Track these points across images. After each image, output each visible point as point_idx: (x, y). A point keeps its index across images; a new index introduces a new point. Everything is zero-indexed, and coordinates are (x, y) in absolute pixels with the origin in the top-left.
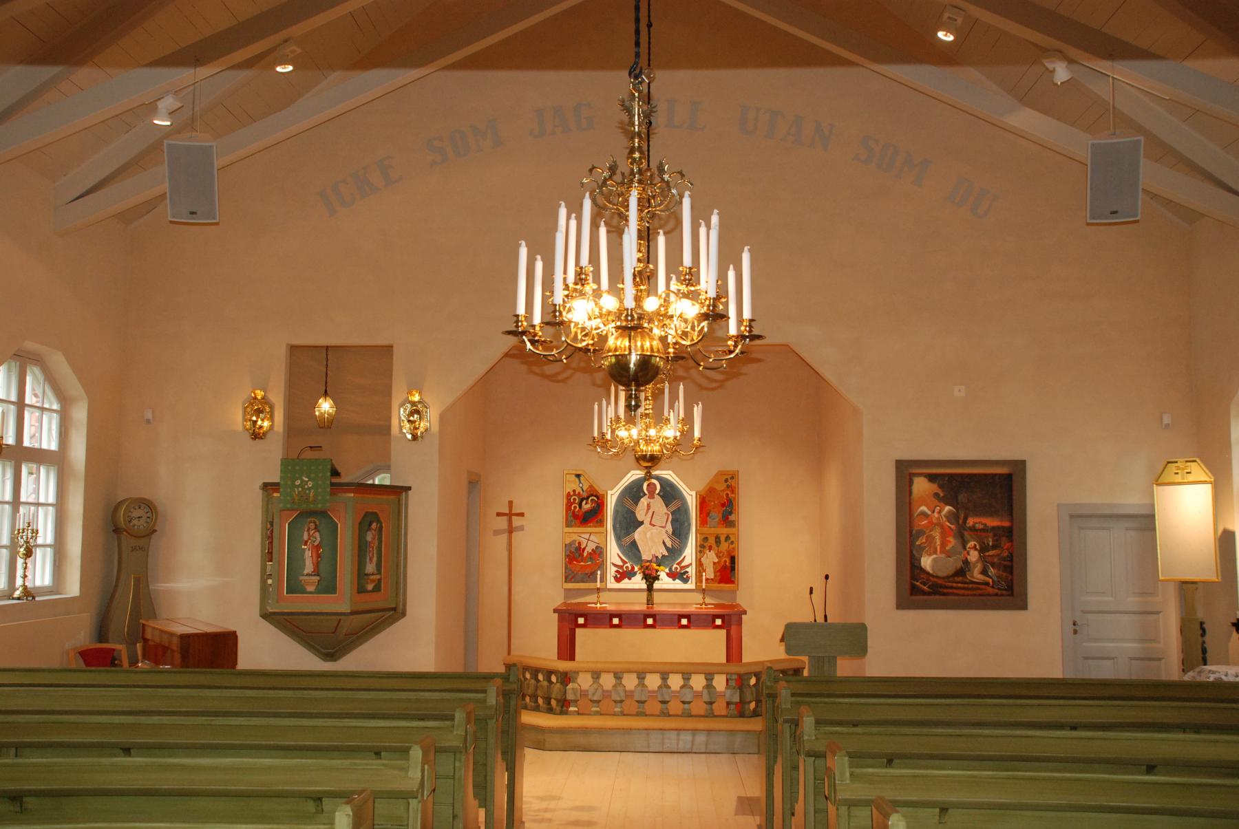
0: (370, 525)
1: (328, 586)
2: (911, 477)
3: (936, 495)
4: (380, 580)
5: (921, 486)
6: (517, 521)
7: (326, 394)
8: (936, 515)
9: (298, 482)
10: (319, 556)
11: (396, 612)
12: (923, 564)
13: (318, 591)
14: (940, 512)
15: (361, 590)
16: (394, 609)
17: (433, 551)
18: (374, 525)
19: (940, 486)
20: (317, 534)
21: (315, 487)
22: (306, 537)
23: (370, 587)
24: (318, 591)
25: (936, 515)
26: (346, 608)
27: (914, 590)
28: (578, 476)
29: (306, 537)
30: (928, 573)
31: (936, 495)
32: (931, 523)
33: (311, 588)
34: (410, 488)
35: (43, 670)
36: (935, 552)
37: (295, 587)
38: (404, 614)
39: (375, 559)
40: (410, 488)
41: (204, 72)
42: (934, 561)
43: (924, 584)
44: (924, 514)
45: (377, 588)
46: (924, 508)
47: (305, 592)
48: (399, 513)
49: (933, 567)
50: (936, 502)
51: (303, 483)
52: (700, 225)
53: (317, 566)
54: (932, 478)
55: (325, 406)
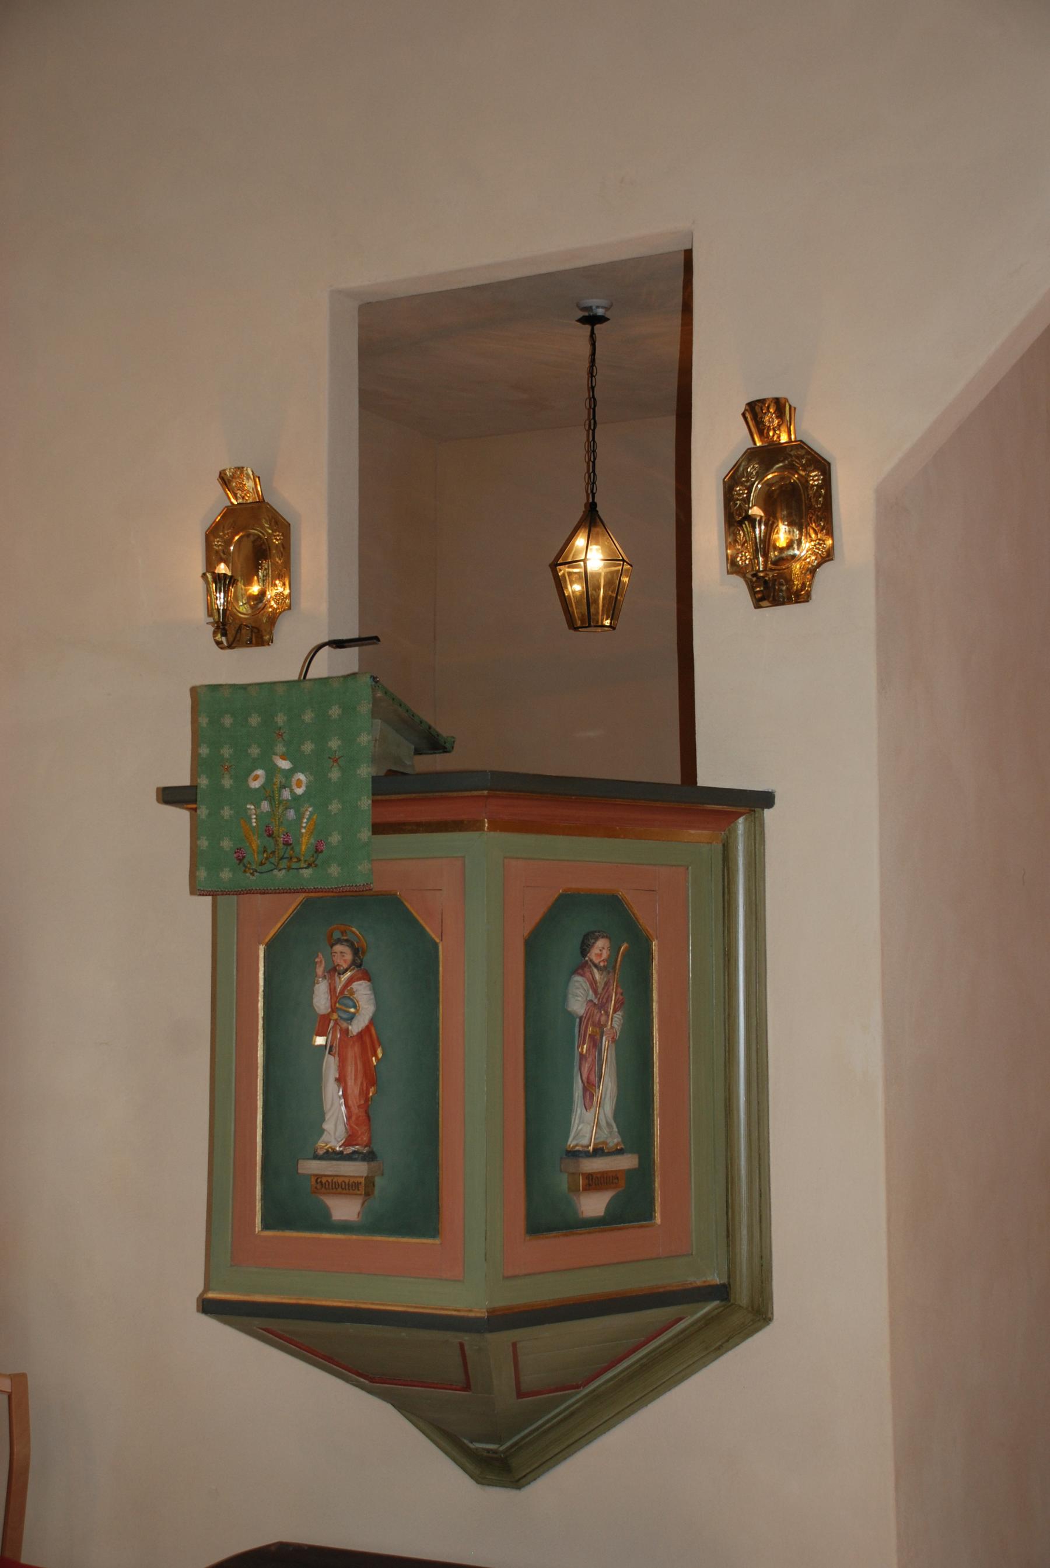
0: (585, 949)
1: (413, 1210)
4: (644, 1174)
6: (245, 861)
7: (591, 520)
9: (257, 780)
10: (370, 1077)
11: (729, 1306)
13: (374, 1224)
15: (546, 1218)
16: (722, 1292)
17: (867, 1051)
18: (600, 949)
20: (362, 990)
21: (318, 793)
22: (321, 1000)
23: (594, 1205)
24: (374, 1224)
26: (467, 1296)
28: (592, 320)
29: (321, 1000)
33: (345, 1209)
34: (767, 799)
37: (291, 1206)
38: (760, 1314)
39: (608, 1088)
40: (767, 799)
45: (633, 1203)
47: (323, 1222)
48: (730, 900)
51: (276, 783)
53: (362, 1116)
55: (593, 557)
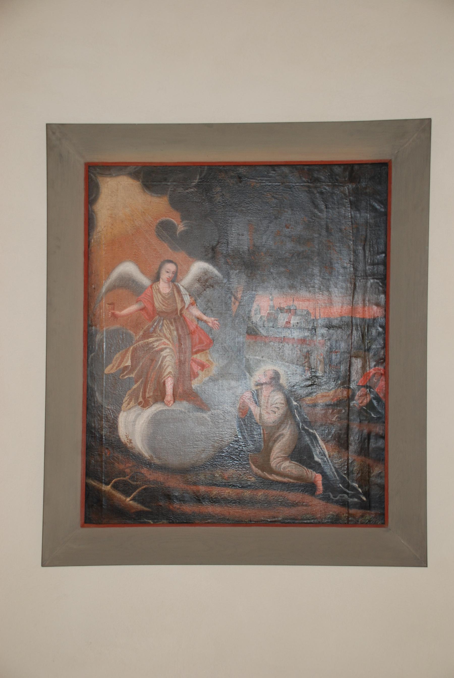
2: (94, 174)
3: (165, 229)
5: (120, 198)
8: (164, 287)
12: (123, 432)
14: (174, 280)
19: (176, 203)
25: (164, 287)
27: (98, 509)
30: (137, 458)
31: (165, 229)
32: (150, 313)
35: (274, 523)
36: (160, 396)
41: (235, 424)
42: (156, 422)
43: (126, 489)
44: (127, 283)
46: (128, 268)
49: (152, 438)
50: (165, 250)
52: (360, 497)
54: (152, 177)
